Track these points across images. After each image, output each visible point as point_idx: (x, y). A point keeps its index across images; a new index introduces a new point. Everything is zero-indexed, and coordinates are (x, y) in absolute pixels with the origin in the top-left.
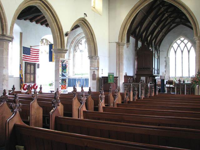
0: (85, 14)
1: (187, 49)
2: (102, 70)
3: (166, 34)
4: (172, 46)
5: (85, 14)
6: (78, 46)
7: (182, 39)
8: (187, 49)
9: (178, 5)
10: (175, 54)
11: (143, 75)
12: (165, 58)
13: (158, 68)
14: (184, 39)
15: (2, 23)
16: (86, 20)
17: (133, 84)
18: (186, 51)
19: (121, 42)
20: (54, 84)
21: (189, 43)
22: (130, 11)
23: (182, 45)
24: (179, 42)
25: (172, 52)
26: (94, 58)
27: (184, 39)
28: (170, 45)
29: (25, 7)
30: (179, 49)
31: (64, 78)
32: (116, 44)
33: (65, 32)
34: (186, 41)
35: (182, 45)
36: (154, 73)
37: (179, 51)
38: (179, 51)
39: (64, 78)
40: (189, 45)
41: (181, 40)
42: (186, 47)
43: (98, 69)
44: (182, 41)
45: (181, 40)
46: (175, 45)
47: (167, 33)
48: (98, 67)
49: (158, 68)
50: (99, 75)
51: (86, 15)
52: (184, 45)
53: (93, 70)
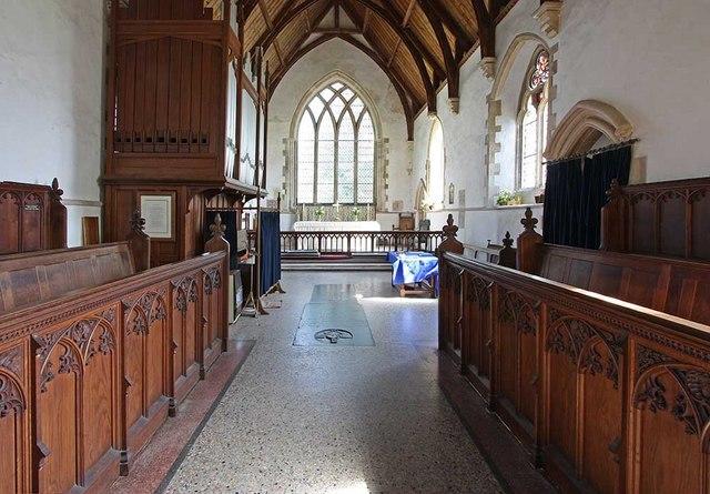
1: (331, 114)
3: (297, 52)
4: (307, 108)
8: (331, 114)
10: (313, 130)
11: (156, 186)
12: (285, 141)
13: (261, 158)
18: (347, 124)
20: (236, 182)
23: (337, 106)
25: (305, 127)
28: (302, 104)
29: (43, 479)
36: (236, 175)
42: (327, 113)
44: (338, 93)
45: (333, 90)
46: (316, 106)
47: (293, 61)
49: (261, 158)
52: (343, 105)
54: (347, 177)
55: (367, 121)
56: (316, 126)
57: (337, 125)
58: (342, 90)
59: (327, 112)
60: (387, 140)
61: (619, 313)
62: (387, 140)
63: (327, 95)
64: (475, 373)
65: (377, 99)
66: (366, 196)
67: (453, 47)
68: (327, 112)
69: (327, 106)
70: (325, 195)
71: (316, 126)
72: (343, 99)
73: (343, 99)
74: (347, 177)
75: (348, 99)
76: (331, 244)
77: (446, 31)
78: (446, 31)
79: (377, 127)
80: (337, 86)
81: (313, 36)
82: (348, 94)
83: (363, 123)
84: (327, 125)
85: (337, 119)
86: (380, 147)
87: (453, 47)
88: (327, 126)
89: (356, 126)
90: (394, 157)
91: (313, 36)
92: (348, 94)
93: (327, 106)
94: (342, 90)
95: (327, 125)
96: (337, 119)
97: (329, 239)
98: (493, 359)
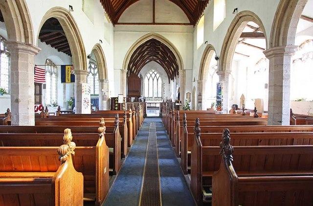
33: (87, 55)
39: (219, 100)
40: (158, 75)
46: (148, 75)
54: (155, 91)
55: (160, 79)
56: (158, 80)
61: (260, 183)
63: (151, 73)
64: (236, 176)
65: (162, 74)
66: (160, 95)
70: (151, 95)
71: (158, 80)
74: (155, 91)
76: (152, 105)
79: (162, 80)
80: (153, 71)
81: (148, 60)
82: (156, 73)
84: (151, 79)
86: (163, 84)
88: (151, 80)
90: (166, 87)
91: (148, 60)
92: (156, 73)
95: (151, 79)
98: (162, 147)
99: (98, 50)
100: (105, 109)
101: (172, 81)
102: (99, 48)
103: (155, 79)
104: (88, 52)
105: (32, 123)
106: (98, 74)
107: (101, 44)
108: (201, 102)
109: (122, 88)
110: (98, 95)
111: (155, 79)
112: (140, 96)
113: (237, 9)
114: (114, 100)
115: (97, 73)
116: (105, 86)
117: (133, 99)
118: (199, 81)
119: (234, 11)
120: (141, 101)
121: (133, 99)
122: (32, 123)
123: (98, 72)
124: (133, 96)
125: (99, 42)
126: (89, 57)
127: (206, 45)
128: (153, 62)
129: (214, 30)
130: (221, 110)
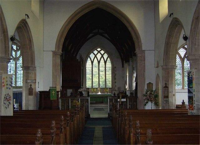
0: (26, 15)
2: (38, 83)
5: (26, 15)
6: (62, 54)
7: (99, 49)
9: (79, 15)
14: (100, 49)
15: (2, 22)
16: (26, 22)
17: (71, 98)
19: (58, 51)
21: (106, 54)
22: (69, 17)
23: (99, 56)
24: (96, 52)
26: (31, 68)
27: (100, 49)
30: (96, 60)
31: (191, 96)
32: (52, 53)
33: (10, 36)
34: (102, 52)
35: (99, 56)
37: (96, 62)
38: (96, 62)
39: (191, 95)
40: (106, 56)
41: (97, 51)
43: (36, 82)
44: (99, 52)
45: (97, 51)
46: (92, 56)
48: (36, 80)
50: (36, 90)
51: (28, 16)
52: (101, 56)
53: (30, 84)
54: (102, 80)
57: (99, 62)
58: (100, 51)
59: (96, 58)
60: (115, 67)
62: (115, 67)
67: (108, 37)
68: (96, 58)
69: (96, 56)
72: (94, 54)
73: (94, 54)
75: (101, 52)
77: (88, 37)
78: (88, 37)
83: (107, 61)
85: (105, 60)
87: (108, 37)
89: (105, 62)
91: (91, 35)
93: (96, 56)
94: (100, 51)
96: (105, 60)
97: (102, 98)
99: (23, 26)
100: (31, 108)
101: (126, 65)
102: (25, 24)
103: (102, 61)
104: (11, 31)
105: (12, 115)
106: (21, 59)
107: (28, 20)
108: (167, 97)
109: (54, 77)
110: (20, 87)
111: (102, 61)
112: (80, 88)
113: (172, 14)
114: (44, 95)
115: (20, 57)
116: (32, 76)
117: (69, 91)
118: (165, 67)
119: (170, 15)
120: (81, 94)
121: (69, 91)
122: (12, 115)
123: (22, 54)
124: (70, 88)
125: (24, 17)
126: (13, 39)
127: (171, 19)
128: (98, 36)
129: (160, 22)
130: (193, 110)
